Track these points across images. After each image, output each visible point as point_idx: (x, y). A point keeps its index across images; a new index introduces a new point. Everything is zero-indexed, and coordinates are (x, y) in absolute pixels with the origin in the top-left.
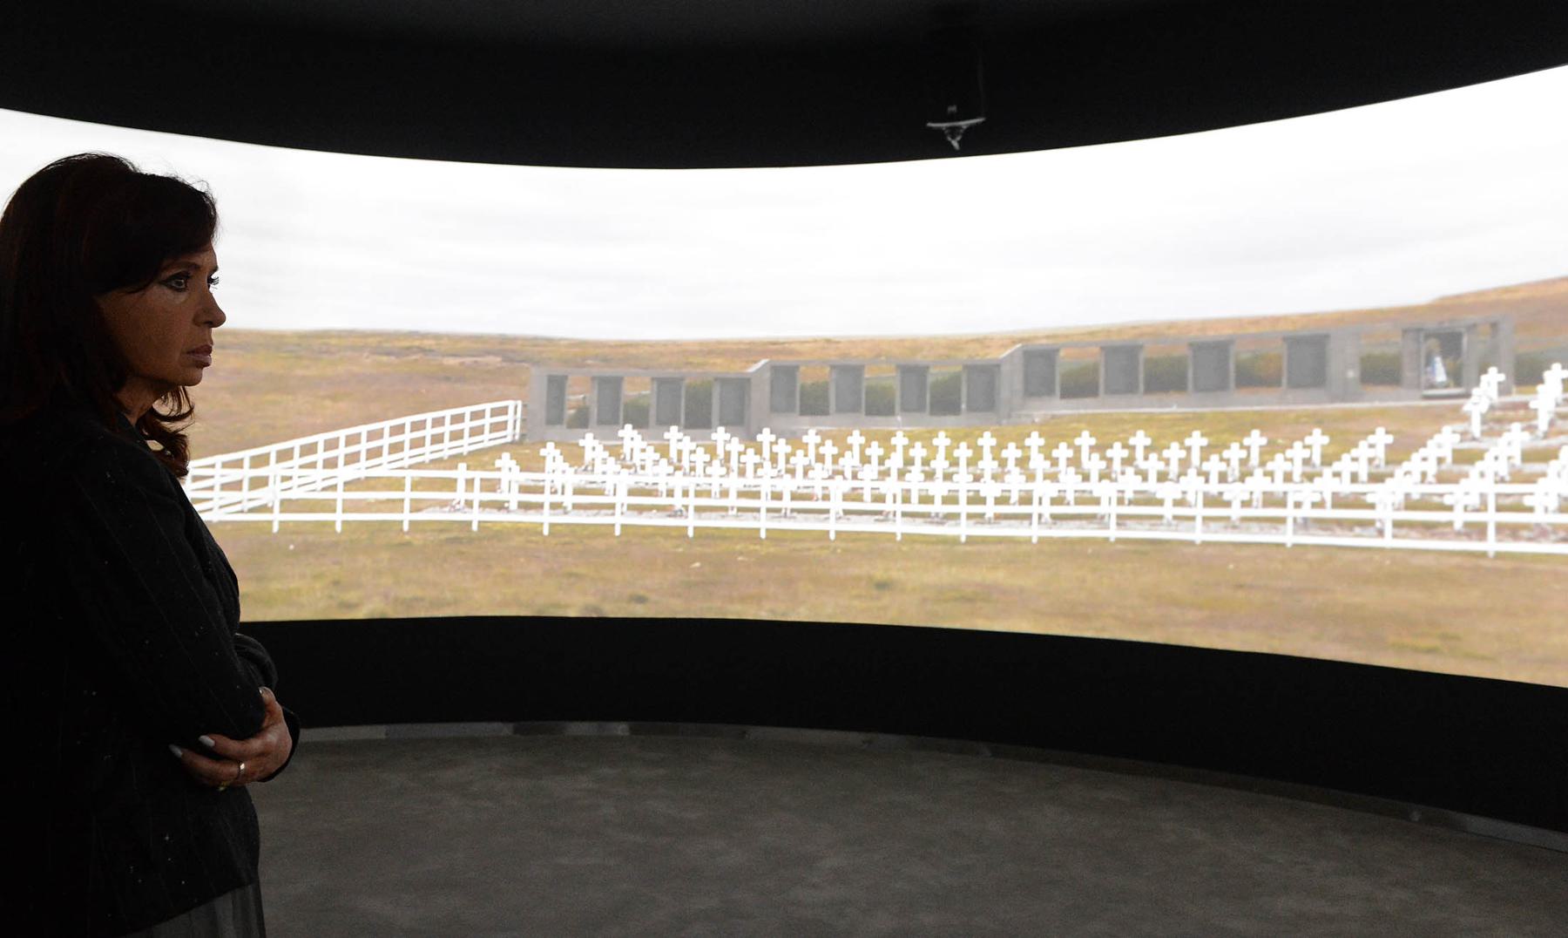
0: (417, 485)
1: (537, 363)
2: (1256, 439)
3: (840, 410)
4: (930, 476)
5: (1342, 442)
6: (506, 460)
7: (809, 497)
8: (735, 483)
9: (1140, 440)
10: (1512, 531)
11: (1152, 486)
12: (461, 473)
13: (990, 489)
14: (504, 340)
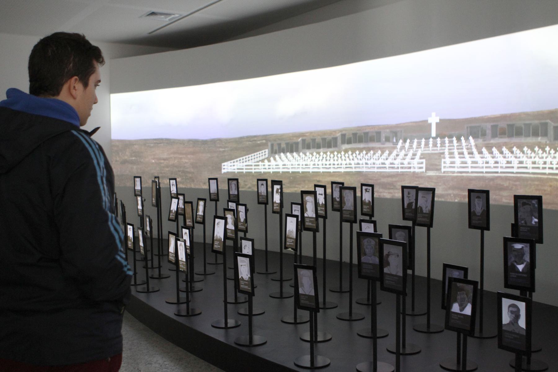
4: (326, 160)
5: (383, 153)
10: (402, 168)
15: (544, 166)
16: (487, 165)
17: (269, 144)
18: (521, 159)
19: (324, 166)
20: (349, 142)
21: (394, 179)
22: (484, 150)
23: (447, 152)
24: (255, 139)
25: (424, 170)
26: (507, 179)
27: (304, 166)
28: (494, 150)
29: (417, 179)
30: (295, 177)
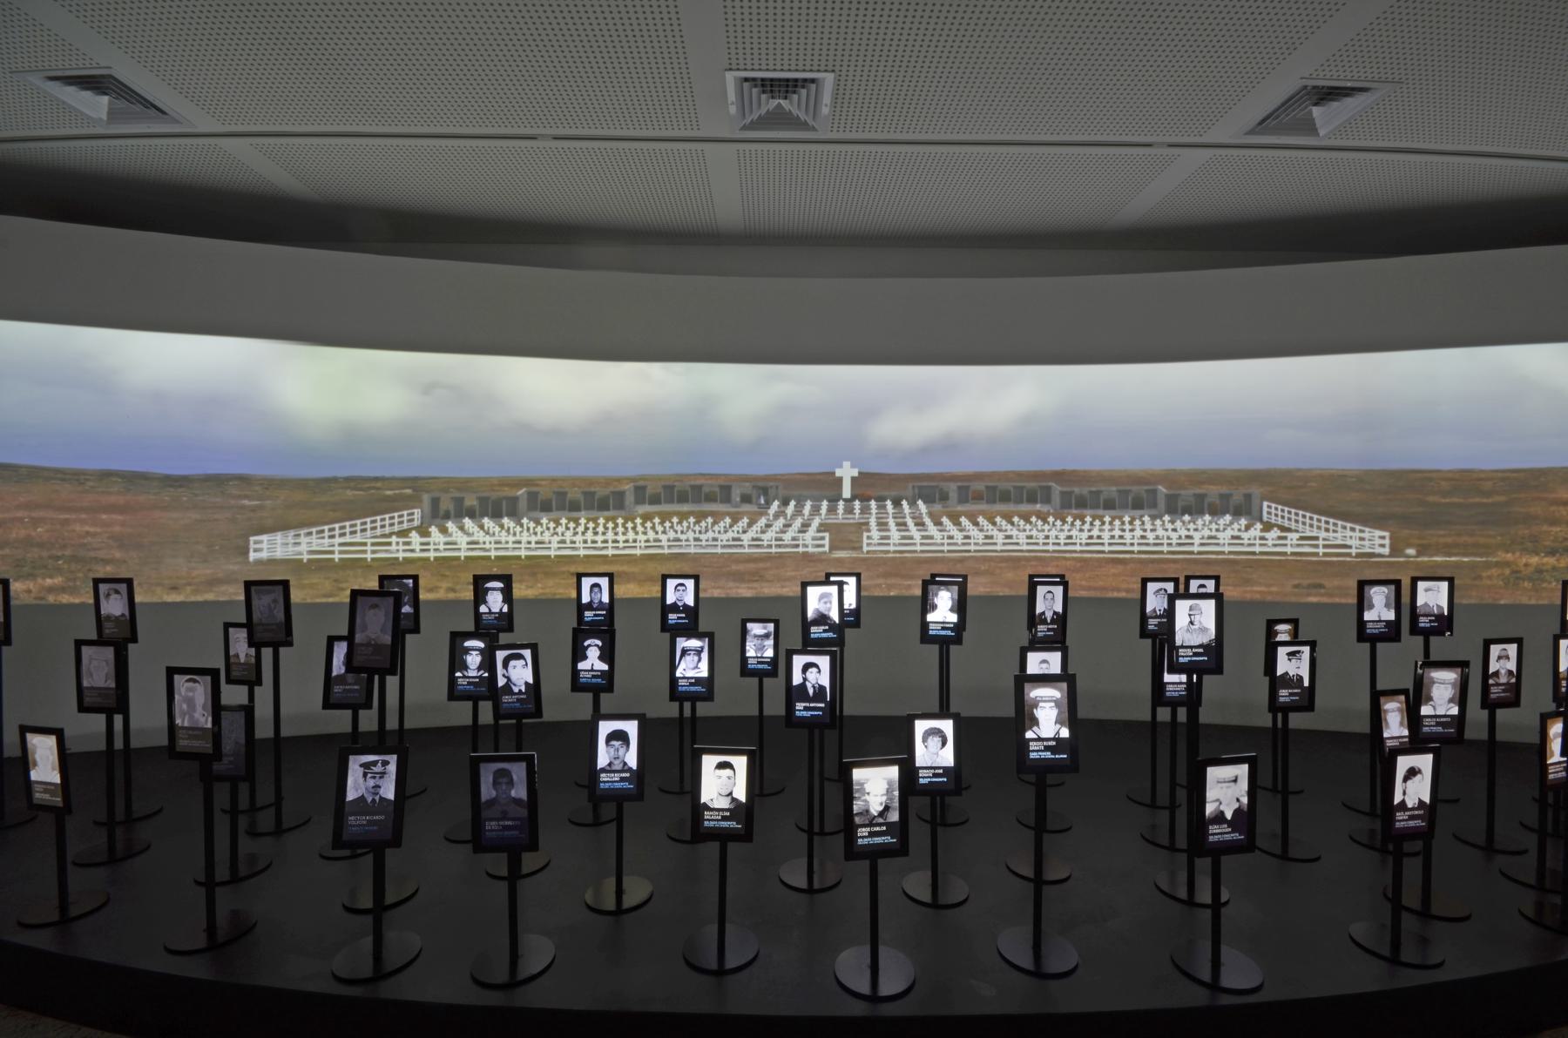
2: (710, 520)
4: (596, 533)
5: (735, 521)
6: (414, 534)
8: (511, 539)
9: (675, 520)
12: (394, 539)
13: (621, 538)
23: (873, 522)
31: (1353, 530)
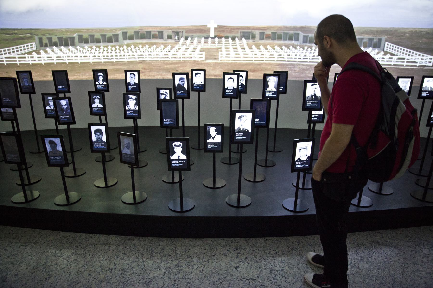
0: (19, 58)
1: (37, 35)
3: (91, 42)
5: (165, 47)
7: (86, 57)
8: (74, 55)
11: (142, 53)
13: (118, 54)
14: (31, 29)
15: (296, 57)
16: (256, 56)
17: (36, 38)
18: (280, 53)
19: (106, 57)
20: (131, 38)
21: (176, 66)
22: (254, 47)
23: (223, 47)
24: (16, 32)
25: (204, 59)
26: (270, 64)
27: (83, 58)
28: (261, 47)
29: (197, 65)
30: (151, 66)
31: (419, 55)
